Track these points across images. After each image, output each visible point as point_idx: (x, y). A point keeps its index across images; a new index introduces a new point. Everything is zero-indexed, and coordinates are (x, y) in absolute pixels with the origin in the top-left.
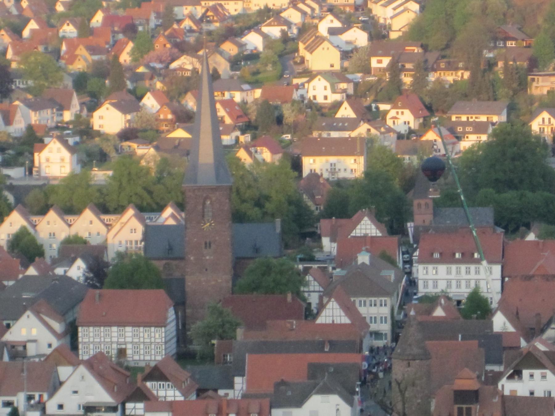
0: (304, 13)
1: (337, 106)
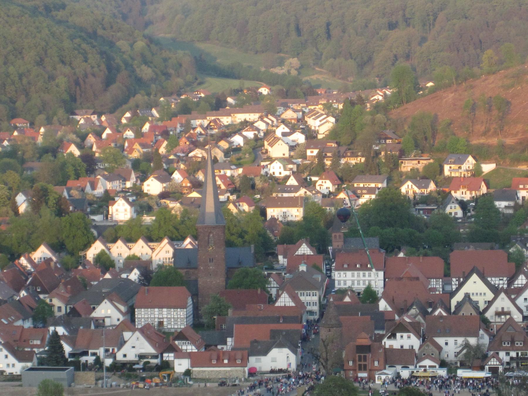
0: (267, 124)
1: (287, 178)
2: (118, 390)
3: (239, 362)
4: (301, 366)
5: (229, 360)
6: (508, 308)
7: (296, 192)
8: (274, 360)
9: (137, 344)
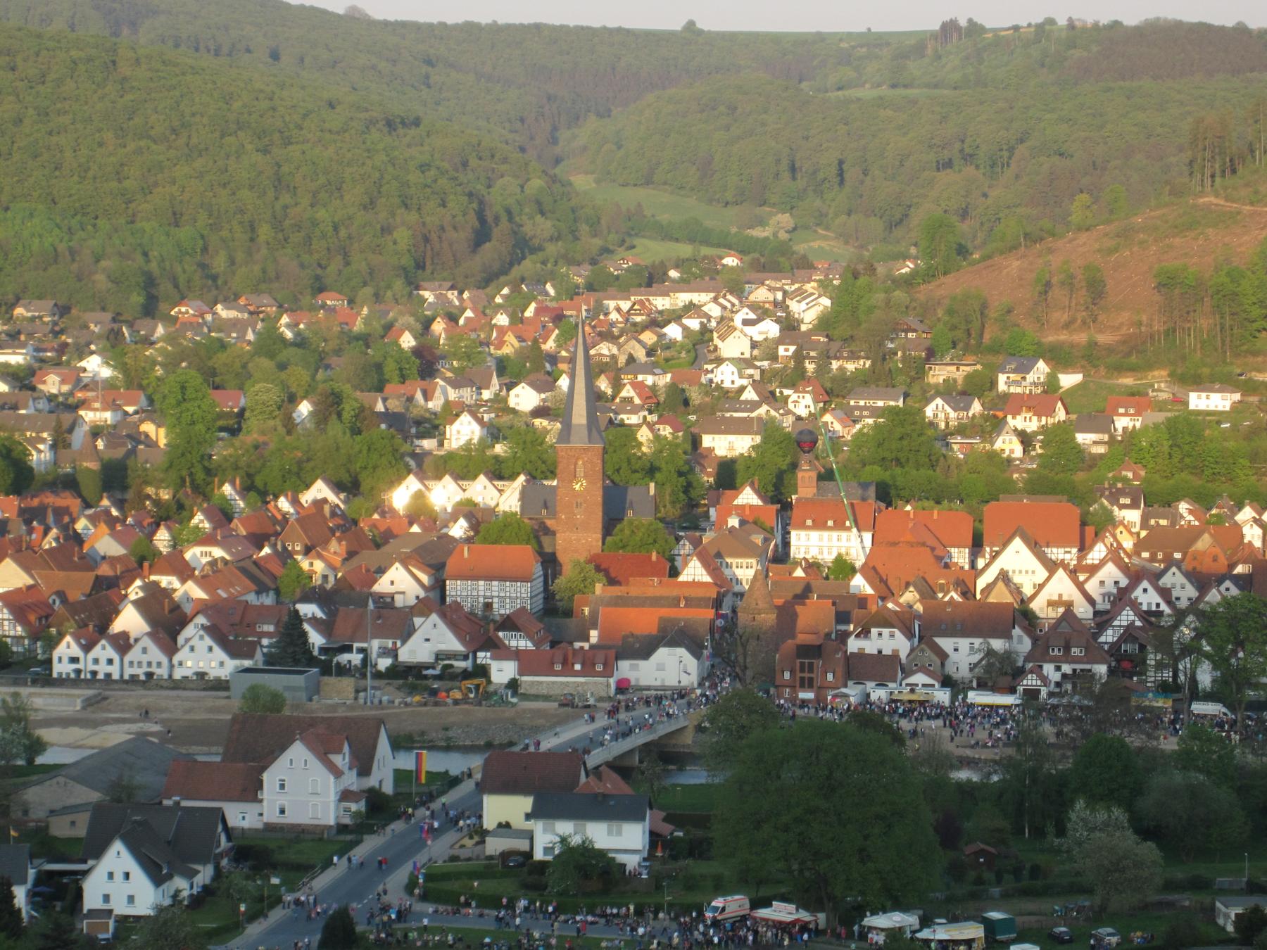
0: (724, 308)
1: (742, 389)
2: (389, 708)
3: (599, 668)
4: (708, 678)
5: (583, 665)
6: (1071, 595)
7: (752, 411)
8: (661, 667)
9: (433, 634)
